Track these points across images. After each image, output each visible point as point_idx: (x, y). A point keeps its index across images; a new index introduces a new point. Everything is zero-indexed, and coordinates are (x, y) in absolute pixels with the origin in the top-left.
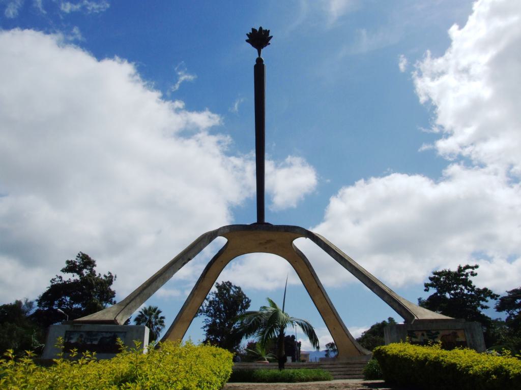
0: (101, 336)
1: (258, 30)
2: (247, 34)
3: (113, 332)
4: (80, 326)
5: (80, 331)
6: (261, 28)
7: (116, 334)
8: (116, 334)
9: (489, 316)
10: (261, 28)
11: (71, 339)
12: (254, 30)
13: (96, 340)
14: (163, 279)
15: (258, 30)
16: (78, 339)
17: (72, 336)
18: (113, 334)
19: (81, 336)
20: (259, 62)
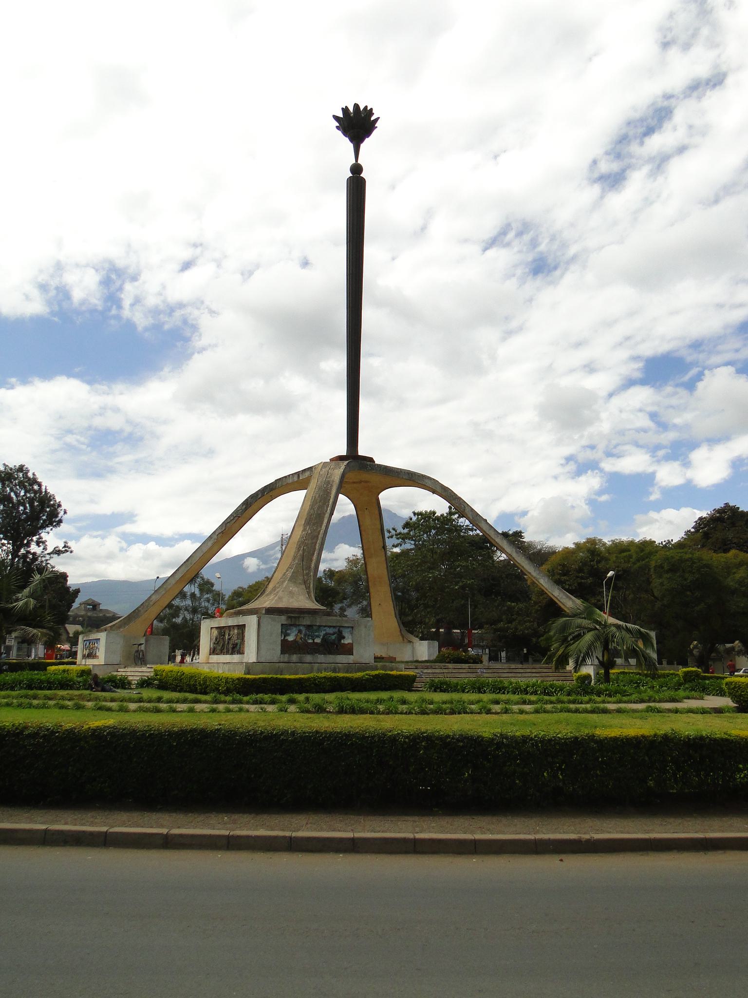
0: (323, 632)
1: (362, 109)
2: (336, 118)
3: (337, 626)
4: (299, 617)
5: (299, 625)
6: (356, 106)
7: (341, 629)
8: (341, 629)
9: (110, 610)
10: (356, 106)
11: (288, 635)
12: (345, 110)
13: (318, 636)
14: (642, 551)
15: (362, 109)
16: (297, 635)
17: (288, 631)
18: (336, 630)
19: (300, 631)
20: (357, 169)
